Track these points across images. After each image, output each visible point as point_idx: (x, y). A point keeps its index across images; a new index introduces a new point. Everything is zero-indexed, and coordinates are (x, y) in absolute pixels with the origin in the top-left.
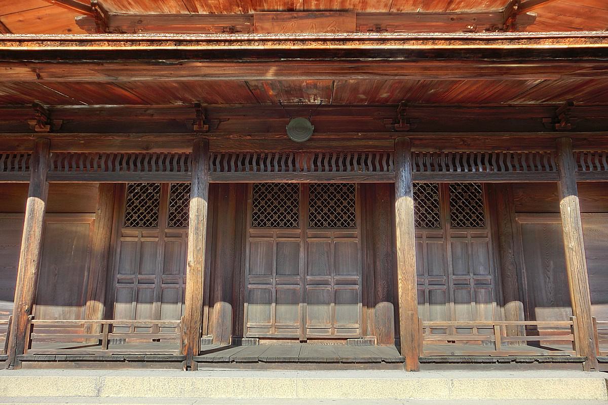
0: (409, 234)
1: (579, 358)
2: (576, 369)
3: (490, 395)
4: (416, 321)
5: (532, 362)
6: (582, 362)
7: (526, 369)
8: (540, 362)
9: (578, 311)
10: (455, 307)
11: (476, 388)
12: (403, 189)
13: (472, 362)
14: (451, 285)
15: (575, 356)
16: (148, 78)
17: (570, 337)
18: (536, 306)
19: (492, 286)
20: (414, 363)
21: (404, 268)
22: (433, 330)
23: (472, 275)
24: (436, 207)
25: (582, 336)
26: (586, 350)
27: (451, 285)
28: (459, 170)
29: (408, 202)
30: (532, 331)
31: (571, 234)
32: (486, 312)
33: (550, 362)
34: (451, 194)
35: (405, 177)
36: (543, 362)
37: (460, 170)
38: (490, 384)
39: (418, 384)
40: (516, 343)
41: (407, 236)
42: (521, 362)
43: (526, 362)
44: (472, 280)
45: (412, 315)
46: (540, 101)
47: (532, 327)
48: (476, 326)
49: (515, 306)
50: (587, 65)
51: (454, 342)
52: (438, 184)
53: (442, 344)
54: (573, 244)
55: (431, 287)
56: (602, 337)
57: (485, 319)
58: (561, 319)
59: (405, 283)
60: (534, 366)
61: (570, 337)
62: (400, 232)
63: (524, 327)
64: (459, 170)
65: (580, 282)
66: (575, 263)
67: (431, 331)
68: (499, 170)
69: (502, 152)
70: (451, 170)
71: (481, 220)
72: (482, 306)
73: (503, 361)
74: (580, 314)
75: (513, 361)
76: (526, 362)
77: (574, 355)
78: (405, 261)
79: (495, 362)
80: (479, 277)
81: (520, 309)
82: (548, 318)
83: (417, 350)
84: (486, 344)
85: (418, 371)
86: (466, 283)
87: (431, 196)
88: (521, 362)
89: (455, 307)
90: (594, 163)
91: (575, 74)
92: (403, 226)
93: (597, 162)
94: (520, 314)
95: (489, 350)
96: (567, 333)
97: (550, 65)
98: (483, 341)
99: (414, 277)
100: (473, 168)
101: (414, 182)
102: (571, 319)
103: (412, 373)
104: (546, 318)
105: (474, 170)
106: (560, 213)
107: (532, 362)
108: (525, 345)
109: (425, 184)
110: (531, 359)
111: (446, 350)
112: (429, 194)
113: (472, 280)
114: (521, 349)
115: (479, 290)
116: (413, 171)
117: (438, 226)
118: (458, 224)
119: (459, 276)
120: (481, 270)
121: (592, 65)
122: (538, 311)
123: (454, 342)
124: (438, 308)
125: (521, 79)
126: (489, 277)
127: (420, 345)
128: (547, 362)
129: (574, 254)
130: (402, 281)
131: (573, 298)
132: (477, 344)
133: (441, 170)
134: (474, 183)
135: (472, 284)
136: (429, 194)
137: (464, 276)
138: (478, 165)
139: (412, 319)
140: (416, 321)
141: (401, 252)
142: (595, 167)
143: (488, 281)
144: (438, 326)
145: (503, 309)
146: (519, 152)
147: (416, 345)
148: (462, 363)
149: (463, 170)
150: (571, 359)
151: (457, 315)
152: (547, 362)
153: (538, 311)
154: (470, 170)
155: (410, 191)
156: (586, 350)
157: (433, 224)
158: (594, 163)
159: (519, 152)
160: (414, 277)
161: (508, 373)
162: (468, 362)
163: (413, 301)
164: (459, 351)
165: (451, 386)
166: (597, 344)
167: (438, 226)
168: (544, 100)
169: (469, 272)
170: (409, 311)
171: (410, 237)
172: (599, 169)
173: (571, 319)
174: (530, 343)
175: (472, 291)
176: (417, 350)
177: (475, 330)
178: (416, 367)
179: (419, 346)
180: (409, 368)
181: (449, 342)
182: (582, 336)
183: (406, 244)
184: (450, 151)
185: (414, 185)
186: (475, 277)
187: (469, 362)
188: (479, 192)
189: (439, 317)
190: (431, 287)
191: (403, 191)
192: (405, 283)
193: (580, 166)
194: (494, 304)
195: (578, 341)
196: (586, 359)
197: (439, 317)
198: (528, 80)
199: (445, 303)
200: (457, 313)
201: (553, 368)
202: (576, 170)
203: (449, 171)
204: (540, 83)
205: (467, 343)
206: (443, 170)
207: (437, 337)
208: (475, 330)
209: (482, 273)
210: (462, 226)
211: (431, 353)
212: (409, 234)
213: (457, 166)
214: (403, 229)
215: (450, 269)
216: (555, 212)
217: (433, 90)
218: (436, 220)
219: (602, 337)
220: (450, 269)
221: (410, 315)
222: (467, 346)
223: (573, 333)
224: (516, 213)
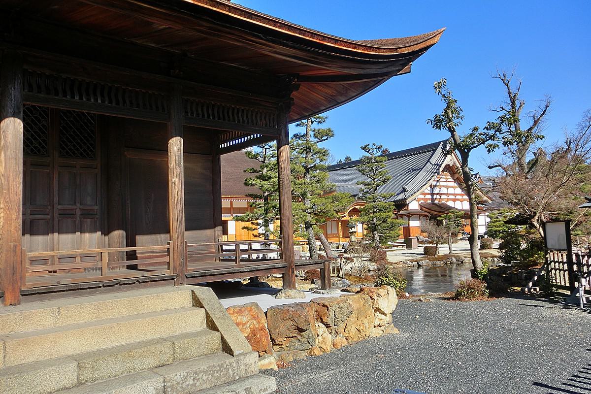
0: (16, 159)
1: (172, 276)
2: (170, 284)
3: (96, 317)
4: (18, 252)
5: (134, 283)
6: (174, 279)
7: (128, 289)
8: (140, 283)
9: (175, 237)
10: (81, 237)
11: (83, 312)
12: (11, 109)
13: (78, 289)
14: (56, 215)
15: (169, 275)
16: (246, 37)
17: (166, 259)
18: (137, 234)
19: (97, 216)
20: (15, 297)
21: (8, 196)
22: (33, 261)
23: (78, 205)
24: (43, 133)
25: (176, 257)
26: (178, 269)
27: (56, 215)
28: (77, 98)
29: (17, 124)
30: (132, 256)
31: (175, 170)
32: (91, 241)
33: (148, 282)
34: (62, 122)
35: (14, 96)
36: (143, 282)
37: (78, 98)
38: (96, 307)
39: (20, 317)
40: (117, 267)
41: (13, 161)
42: (124, 284)
43: (129, 284)
44: (78, 210)
45: (15, 246)
46: (160, 46)
47: (132, 253)
48: (80, 254)
49: (118, 235)
50: (205, 24)
51: (55, 272)
52: (48, 108)
53: (42, 274)
54: (175, 179)
55: (33, 217)
56: (190, 257)
57: (89, 247)
58: (156, 244)
59: (8, 212)
60: (135, 287)
61: (166, 259)
62: (5, 156)
63: (125, 253)
64: (77, 98)
65: (178, 212)
66: (176, 195)
67: (59, 261)
68: (118, 103)
69: (93, 82)
70: (68, 96)
71: (91, 151)
72: (87, 235)
73: (108, 284)
74: (176, 239)
75: (117, 284)
76: (129, 284)
77: (168, 273)
78: (9, 189)
79: (100, 287)
80: (86, 208)
81: (123, 237)
82: (146, 244)
83: (19, 283)
84: (89, 271)
85: (19, 304)
86: (72, 212)
87: (39, 121)
88: (124, 284)
89: (58, 237)
90: (197, 111)
91: (195, 29)
92: (9, 150)
93: (200, 110)
94: (123, 242)
95: (95, 276)
96: (165, 256)
97: (176, 14)
98: (85, 269)
99: (19, 206)
100: (92, 98)
101: (24, 102)
102: (169, 244)
103: (12, 307)
104: (144, 244)
105: (92, 100)
106: (168, 151)
107: (134, 283)
108: (125, 269)
109: (33, 106)
110: (133, 280)
111: (51, 281)
112: (36, 118)
113: (78, 210)
114: (122, 273)
115: (85, 220)
116: (24, 90)
117: (45, 153)
118: (67, 153)
119: (65, 206)
120: (89, 200)
121: (208, 25)
122: (139, 238)
123: (55, 272)
124: (40, 239)
125: (150, 20)
126: (96, 207)
127: (22, 278)
128: (147, 282)
129: (176, 187)
130: (4, 210)
131: (171, 225)
132: (79, 272)
133: (57, 94)
134: (88, 113)
135: (78, 214)
136: (36, 118)
137: (70, 206)
138: (97, 96)
139: (15, 251)
140: (18, 252)
141: (5, 179)
142: (198, 115)
143: (94, 211)
144: (39, 257)
145: (106, 238)
146: (137, 90)
147: (17, 278)
148: (67, 291)
149: (81, 98)
150: (165, 277)
151: (60, 246)
152: (147, 282)
153: (139, 238)
154: (89, 100)
155: (20, 112)
156: (178, 269)
157: (39, 151)
158: (197, 111)
159: (137, 90)
160: (19, 206)
161: (113, 295)
162: (73, 290)
163: (17, 231)
164: (66, 280)
165: (57, 315)
166: (186, 263)
167: (45, 153)
168: (164, 45)
169: (75, 203)
170: (11, 242)
171: (16, 163)
172: (201, 116)
173: (169, 244)
174: (129, 267)
175: (77, 222)
176: (19, 283)
177: (78, 259)
178: (16, 300)
179: (21, 278)
180: (8, 302)
181: (50, 272)
182: (175, 258)
183: (12, 170)
184: (69, 76)
185: (24, 105)
186: (81, 207)
187: (76, 289)
188: (91, 123)
189: (40, 247)
190: (33, 217)
191: (11, 111)
192: (8, 212)
193: (187, 113)
194: (99, 233)
195: (172, 263)
196: (178, 276)
197: (40, 247)
198: (155, 23)
199: (48, 234)
200: (60, 242)
201: (151, 286)
202: (183, 114)
203: (111, 104)
204: (164, 29)
205: (69, 271)
206: (60, 95)
207: (36, 268)
208: (78, 259)
209: (89, 203)
210: (37, 154)
211: (35, 284)
212: (16, 159)
213: (75, 93)
214: (8, 153)
215: (56, 199)
216: (164, 150)
217: (56, 7)
218: (43, 147)
219: (190, 257)
220: (56, 199)
221: (12, 246)
222: (69, 274)
223: (169, 255)
224: (126, 147)
